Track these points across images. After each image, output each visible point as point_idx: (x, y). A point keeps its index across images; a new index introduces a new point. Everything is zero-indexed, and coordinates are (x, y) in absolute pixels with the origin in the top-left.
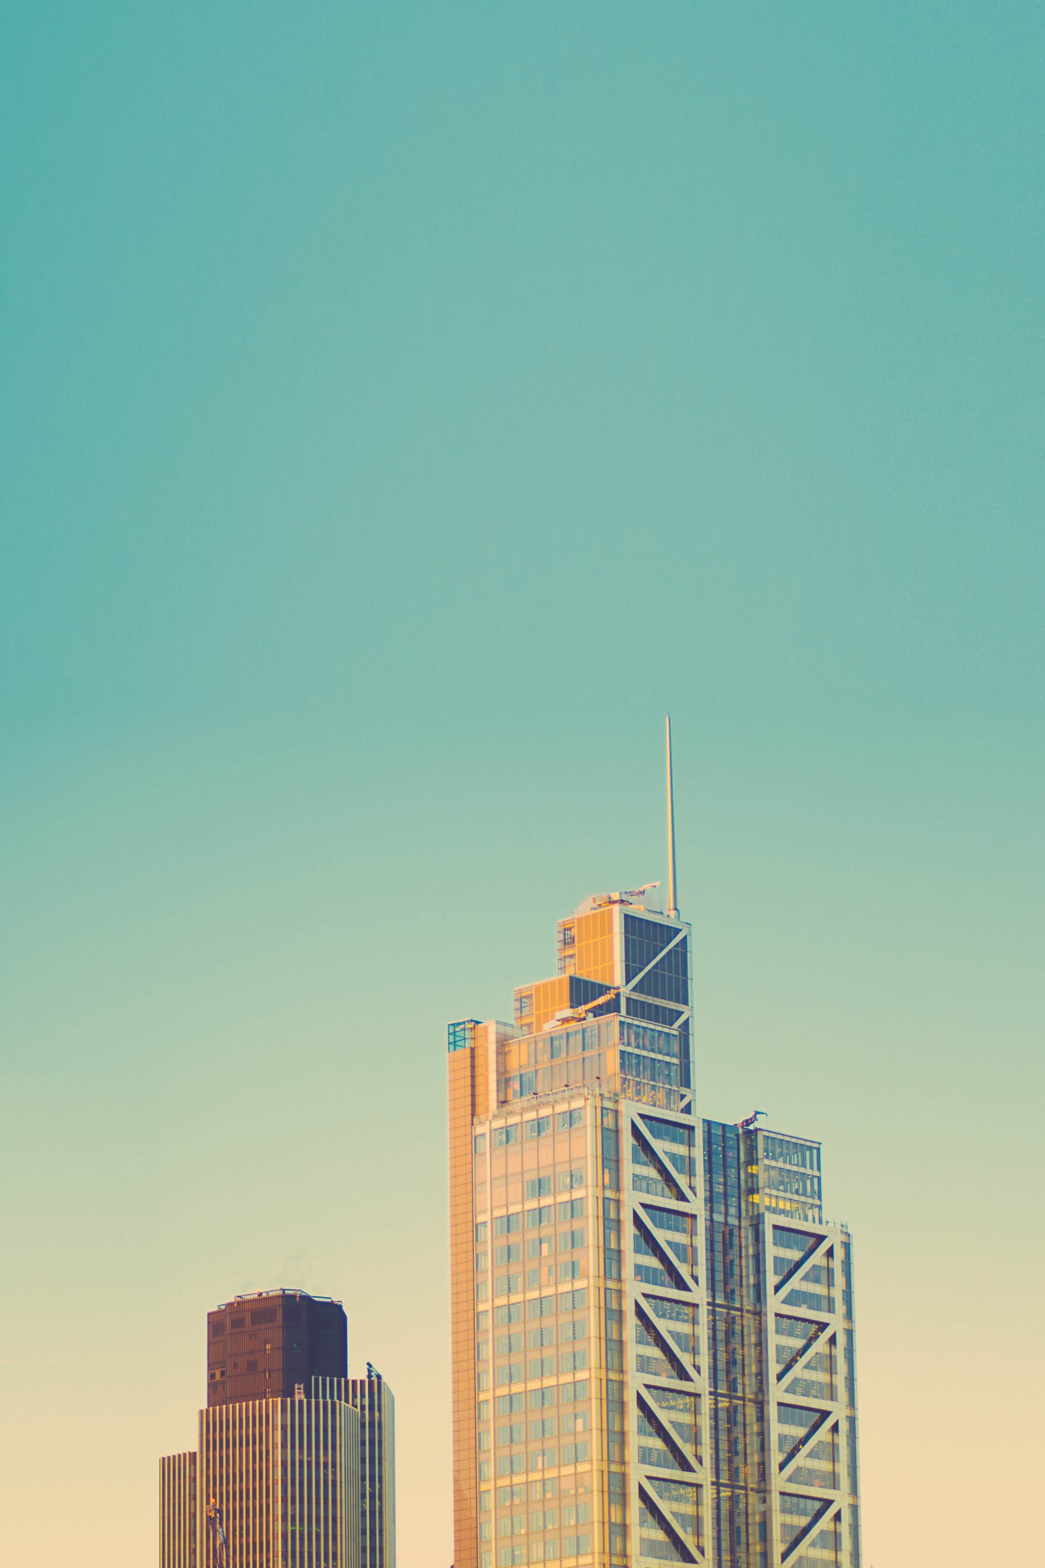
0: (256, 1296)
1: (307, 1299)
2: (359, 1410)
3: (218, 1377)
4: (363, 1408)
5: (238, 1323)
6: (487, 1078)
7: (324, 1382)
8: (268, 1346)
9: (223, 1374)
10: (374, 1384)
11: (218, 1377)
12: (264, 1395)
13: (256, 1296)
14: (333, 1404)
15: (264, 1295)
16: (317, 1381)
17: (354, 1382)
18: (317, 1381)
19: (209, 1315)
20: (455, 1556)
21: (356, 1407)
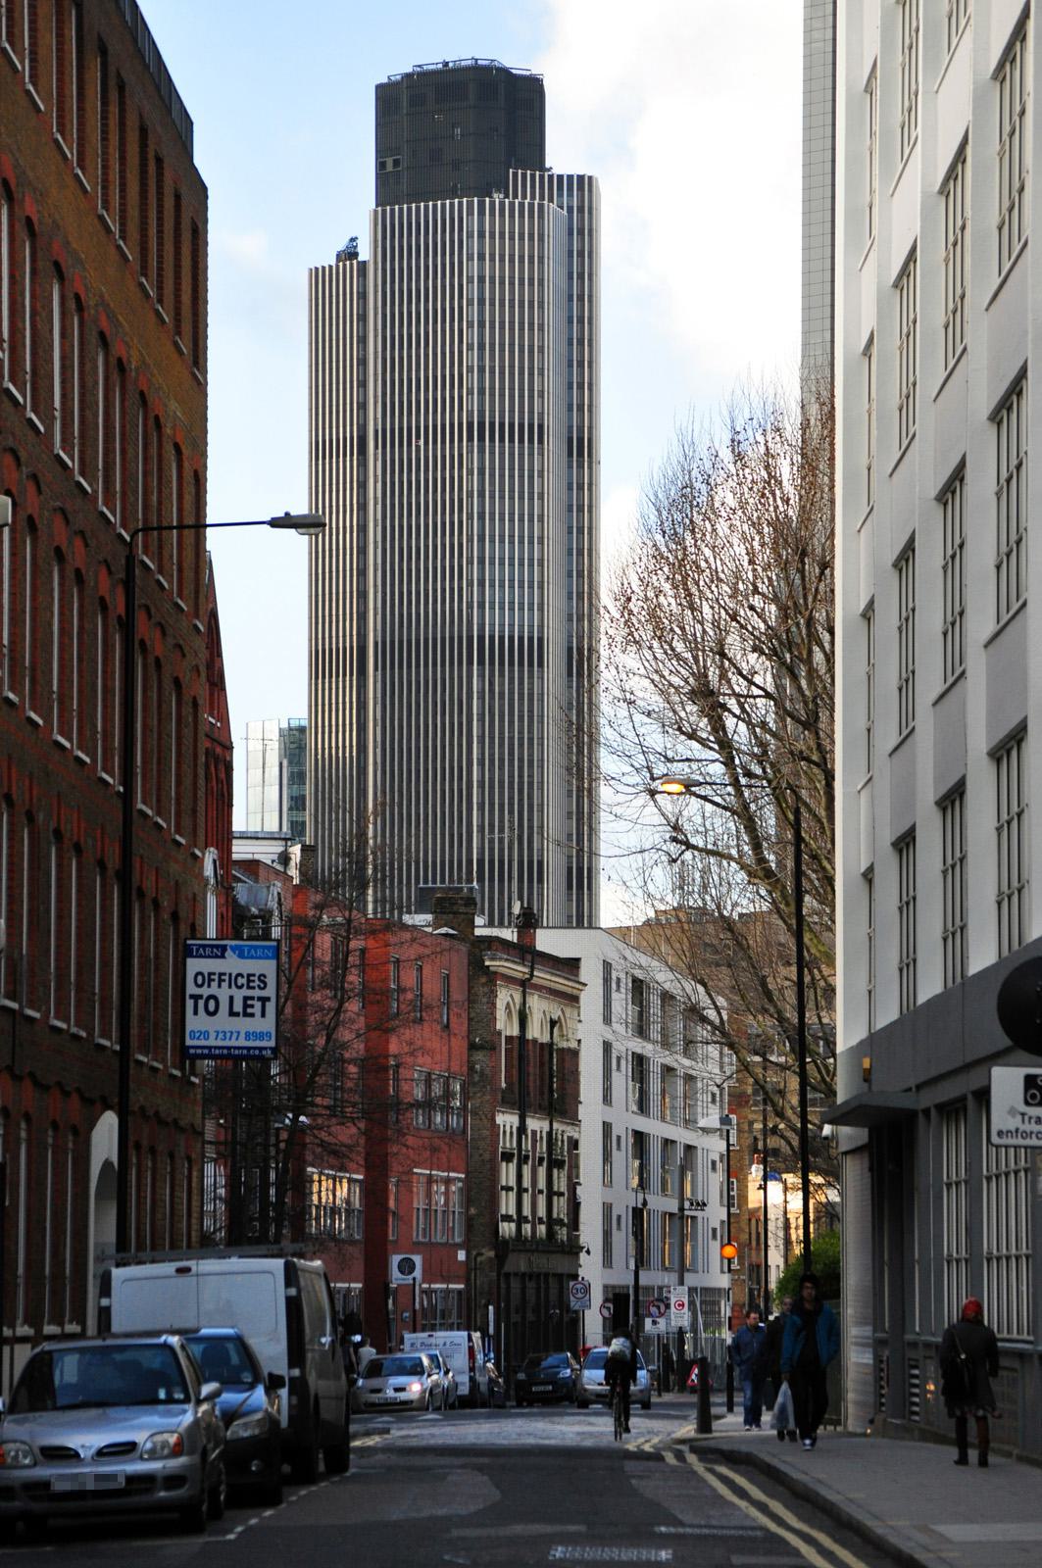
0: (440, 66)
1: (505, 72)
2: (565, 212)
3: (390, 168)
4: (570, 210)
5: (417, 100)
6: (402, 1429)
7: (524, 176)
8: (458, 131)
9: (396, 163)
10: (583, 185)
11: (390, 168)
12: (453, 194)
13: (440, 66)
14: (541, 206)
15: (451, 65)
16: (515, 175)
17: (560, 177)
18: (515, 175)
19: (379, 88)
20: (804, 160)
21: (562, 208)
